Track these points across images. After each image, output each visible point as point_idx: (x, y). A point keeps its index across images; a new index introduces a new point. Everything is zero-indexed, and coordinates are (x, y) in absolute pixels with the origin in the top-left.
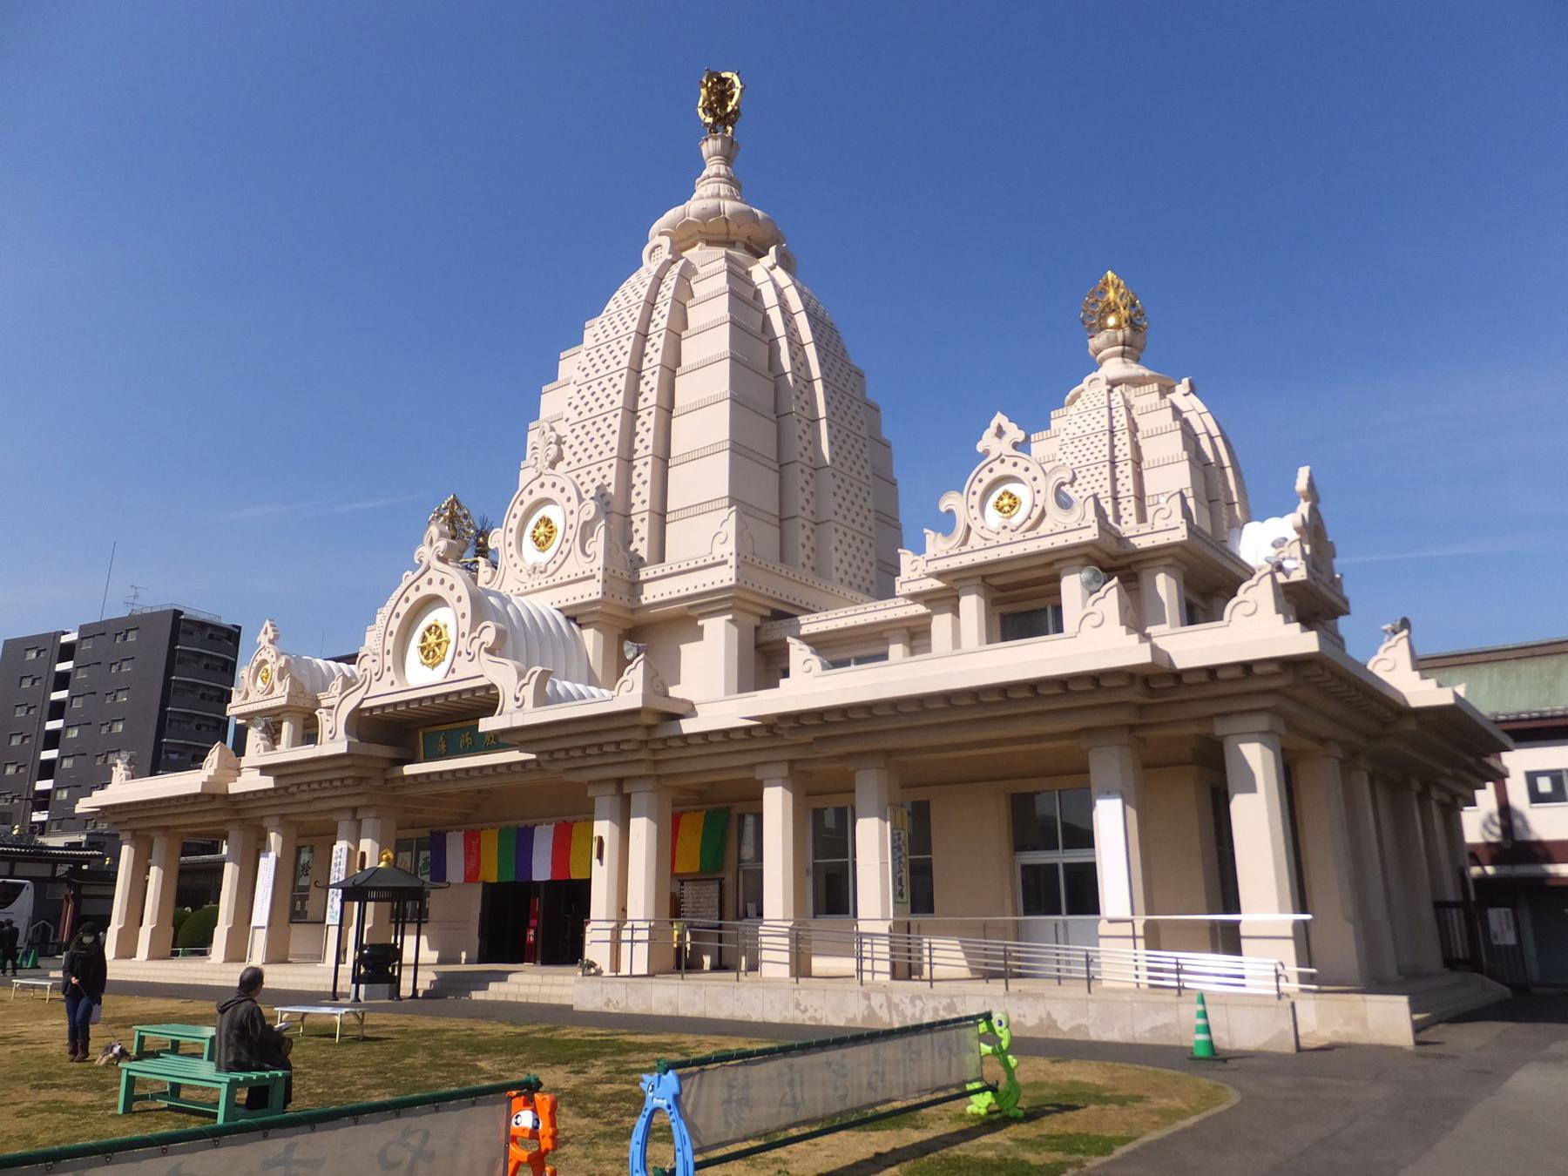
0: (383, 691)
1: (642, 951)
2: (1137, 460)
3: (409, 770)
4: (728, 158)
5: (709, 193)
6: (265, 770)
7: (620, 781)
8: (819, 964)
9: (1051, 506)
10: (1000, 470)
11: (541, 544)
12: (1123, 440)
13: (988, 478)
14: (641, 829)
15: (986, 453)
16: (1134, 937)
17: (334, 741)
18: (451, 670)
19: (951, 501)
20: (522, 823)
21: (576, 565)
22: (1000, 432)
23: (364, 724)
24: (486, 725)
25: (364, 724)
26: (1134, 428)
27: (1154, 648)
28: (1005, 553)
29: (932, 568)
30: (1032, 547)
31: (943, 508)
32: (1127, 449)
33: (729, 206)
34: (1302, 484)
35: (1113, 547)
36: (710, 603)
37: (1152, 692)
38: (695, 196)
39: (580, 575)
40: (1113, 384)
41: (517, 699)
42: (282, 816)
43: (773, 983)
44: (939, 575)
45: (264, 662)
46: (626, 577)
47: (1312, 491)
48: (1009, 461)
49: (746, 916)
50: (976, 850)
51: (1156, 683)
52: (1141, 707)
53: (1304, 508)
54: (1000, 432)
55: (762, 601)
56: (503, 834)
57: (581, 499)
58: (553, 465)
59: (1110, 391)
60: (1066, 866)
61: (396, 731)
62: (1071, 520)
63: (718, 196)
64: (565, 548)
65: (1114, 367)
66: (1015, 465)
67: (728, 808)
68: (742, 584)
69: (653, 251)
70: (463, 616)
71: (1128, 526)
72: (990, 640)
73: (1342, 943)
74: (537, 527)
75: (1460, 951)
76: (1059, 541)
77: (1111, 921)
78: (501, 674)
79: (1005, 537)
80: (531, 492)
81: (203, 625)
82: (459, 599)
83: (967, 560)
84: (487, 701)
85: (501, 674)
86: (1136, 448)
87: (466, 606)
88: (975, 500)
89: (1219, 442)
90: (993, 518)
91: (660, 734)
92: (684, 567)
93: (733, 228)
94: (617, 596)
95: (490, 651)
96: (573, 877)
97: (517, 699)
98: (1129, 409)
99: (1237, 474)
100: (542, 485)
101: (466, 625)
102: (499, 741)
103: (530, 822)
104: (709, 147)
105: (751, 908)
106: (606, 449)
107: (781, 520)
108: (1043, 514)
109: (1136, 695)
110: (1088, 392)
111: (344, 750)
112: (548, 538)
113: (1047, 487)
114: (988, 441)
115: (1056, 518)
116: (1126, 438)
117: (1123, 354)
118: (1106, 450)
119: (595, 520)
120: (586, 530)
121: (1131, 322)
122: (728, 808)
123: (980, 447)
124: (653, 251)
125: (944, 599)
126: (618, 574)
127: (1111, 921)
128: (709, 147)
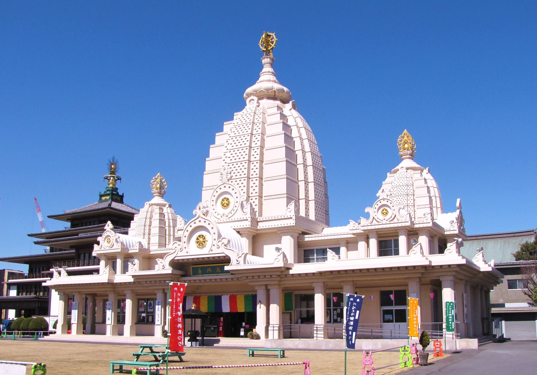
1: (276, 333)
4: (272, 65)
5: (267, 80)
6: (133, 276)
10: (383, 202)
13: (380, 204)
17: (163, 268)
21: (239, 215)
23: (177, 265)
24: (226, 268)
25: (177, 265)
28: (384, 226)
29: (363, 228)
30: (111, 251)
31: (366, 211)
33: (267, 80)
34: (458, 204)
40: (407, 169)
42: (132, 290)
44: (364, 230)
45: (108, 236)
47: (460, 207)
49: (297, 323)
51: (111, 285)
52: (423, 273)
53: (458, 211)
54: (108, 226)
56: (209, 298)
60: (395, 310)
61: (182, 267)
63: (270, 81)
64: (235, 209)
67: (292, 293)
69: (250, 101)
75: (486, 331)
79: (384, 222)
90: (380, 216)
91: (285, 273)
93: (277, 94)
96: (239, 311)
100: (225, 187)
103: (220, 294)
106: (243, 174)
109: (423, 271)
110: (400, 171)
111: (171, 272)
112: (228, 205)
122: (292, 293)
123: (377, 195)
124: (250, 101)
125: (366, 237)
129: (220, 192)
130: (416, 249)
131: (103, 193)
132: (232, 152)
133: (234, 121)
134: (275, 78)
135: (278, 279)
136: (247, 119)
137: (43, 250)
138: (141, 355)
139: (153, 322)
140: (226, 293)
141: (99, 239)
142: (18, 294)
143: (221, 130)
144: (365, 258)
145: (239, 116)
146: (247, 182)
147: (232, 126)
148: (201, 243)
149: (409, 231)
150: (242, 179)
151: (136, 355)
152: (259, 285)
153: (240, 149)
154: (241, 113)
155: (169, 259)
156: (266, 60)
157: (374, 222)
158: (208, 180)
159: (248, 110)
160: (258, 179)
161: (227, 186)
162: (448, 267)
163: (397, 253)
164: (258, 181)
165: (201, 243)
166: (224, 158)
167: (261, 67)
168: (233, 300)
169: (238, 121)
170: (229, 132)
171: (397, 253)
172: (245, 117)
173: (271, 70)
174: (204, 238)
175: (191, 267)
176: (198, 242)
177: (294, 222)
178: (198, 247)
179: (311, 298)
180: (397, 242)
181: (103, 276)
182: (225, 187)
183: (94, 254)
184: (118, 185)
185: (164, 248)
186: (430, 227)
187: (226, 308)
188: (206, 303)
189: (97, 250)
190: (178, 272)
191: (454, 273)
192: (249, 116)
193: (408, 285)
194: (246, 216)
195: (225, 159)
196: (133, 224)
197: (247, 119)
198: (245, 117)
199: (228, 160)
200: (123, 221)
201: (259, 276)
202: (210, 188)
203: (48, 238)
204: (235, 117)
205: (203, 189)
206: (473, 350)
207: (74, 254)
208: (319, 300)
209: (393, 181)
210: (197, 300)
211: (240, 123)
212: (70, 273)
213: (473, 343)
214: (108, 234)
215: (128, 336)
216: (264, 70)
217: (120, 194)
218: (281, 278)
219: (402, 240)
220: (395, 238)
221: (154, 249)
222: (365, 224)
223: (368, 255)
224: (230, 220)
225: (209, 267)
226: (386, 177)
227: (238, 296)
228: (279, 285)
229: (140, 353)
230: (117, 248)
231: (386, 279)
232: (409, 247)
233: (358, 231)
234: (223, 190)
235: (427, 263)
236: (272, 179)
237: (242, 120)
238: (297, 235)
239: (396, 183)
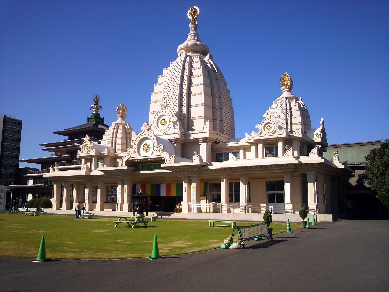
0: (135, 157)
3: (142, 172)
4: (195, 28)
5: (190, 40)
6: (102, 171)
8: (105, 210)
9: (278, 129)
10: (268, 121)
11: (164, 124)
13: (265, 122)
14: (194, 185)
15: (265, 118)
16: (291, 206)
17: (122, 166)
18: (152, 153)
19: (258, 126)
21: (172, 130)
22: (87, 138)
23: (129, 163)
24: (162, 165)
25: (129, 163)
28: (268, 137)
29: (254, 139)
30: (274, 137)
31: (256, 128)
34: (321, 122)
35: (288, 137)
36: (203, 140)
37: (296, 167)
38: (188, 39)
39: (172, 133)
40: (286, 98)
41: (170, 161)
43: (225, 214)
44: (255, 140)
45: (87, 144)
46: (183, 133)
47: (323, 124)
48: (269, 120)
50: (261, 190)
53: (322, 126)
54: (87, 138)
55: (212, 139)
57: (173, 116)
58: (165, 107)
59: (286, 100)
61: (135, 165)
64: (170, 126)
65: (286, 94)
66: (271, 120)
68: (210, 137)
69: (181, 54)
70: (155, 143)
73: (323, 206)
74: (162, 120)
76: (279, 136)
77: (287, 204)
78: (166, 155)
80: (160, 113)
81: (12, 120)
82: (153, 139)
83: (261, 138)
84: (163, 161)
85: (166, 155)
87: (155, 140)
88: (263, 126)
91: (201, 169)
92: (199, 132)
94: (182, 137)
95: (162, 150)
97: (170, 161)
98: (290, 104)
100: (163, 112)
101: (156, 144)
102: (164, 168)
103: (159, 183)
104: (191, 26)
106: (175, 103)
107: (213, 120)
108: (276, 131)
114: (265, 115)
115: (279, 132)
119: (177, 121)
120: (175, 123)
123: (264, 116)
124: (181, 54)
126: (182, 133)
127: (287, 204)
128: (191, 26)
129: (159, 115)
130: (290, 151)
131: (90, 117)
132: (168, 88)
133: (170, 68)
135: (197, 173)
136: (178, 66)
137: (49, 155)
138: (119, 222)
139: (96, 202)
141: (81, 147)
142: (34, 183)
143: (162, 74)
144: (253, 159)
145: (173, 64)
146: (165, 111)
147: (168, 70)
149: (286, 141)
150: (175, 107)
151: (116, 222)
153: (171, 87)
154: (175, 62)
155: (125, 159)
158: (154, 107)
159: (180, 60)
160: (285, 116)
162: (311, 165)
163: (277, 155)
164: (285, 117)
166: (163, 92)
167: (190, 31)
168: (168, 187)
169: (173, 67)
170: (167, 75)
171: (277, 155)
172: (177, 65)
177: (209, 135)
178: (147, 152)
179: (219, 186)
180: (277, 148)
184: (100, 112)
185: (125, 153)
186: (300, 138)
187: (163, 193)
188: (150, 188)
189: (79, 154)
190: (132, 168)
191: (315, 169)
192: (180, 64)
194: (177, 131)
195: (164, 93)
196: (104, 137)
197: (178, 66)
198: (177, 65)
199: (165, 94)
200: (97, 134)
201: (184, 171)
202: (153, 112)
203: (50, 147)
204: (171, 65)
205: (150, 113)
206: (328, 223)
207: (69, 157)
208: (223, 186)
209: (277, 107)
210: (143, 187)
211: (174, 69)
213: (329, 218)
214: (87, 143)
215: (97, 211)
216: (191, 32)
217: (102, 118)
218: (199, 172)
220: (276, 145)
221: (119, 154)
222: (255, 136)
223: (257, 156)
224: (166, 134)
227: (171, 185)
228: (198, 177)
229: (118, 221)
230: (93, 153)
231: (256, 174)
232: (285, 151)
233: (251, 141)
234: (162, 114)
236: (196, 106)
237: (175, 67)
238: (211, 144)
239: (278, 108)
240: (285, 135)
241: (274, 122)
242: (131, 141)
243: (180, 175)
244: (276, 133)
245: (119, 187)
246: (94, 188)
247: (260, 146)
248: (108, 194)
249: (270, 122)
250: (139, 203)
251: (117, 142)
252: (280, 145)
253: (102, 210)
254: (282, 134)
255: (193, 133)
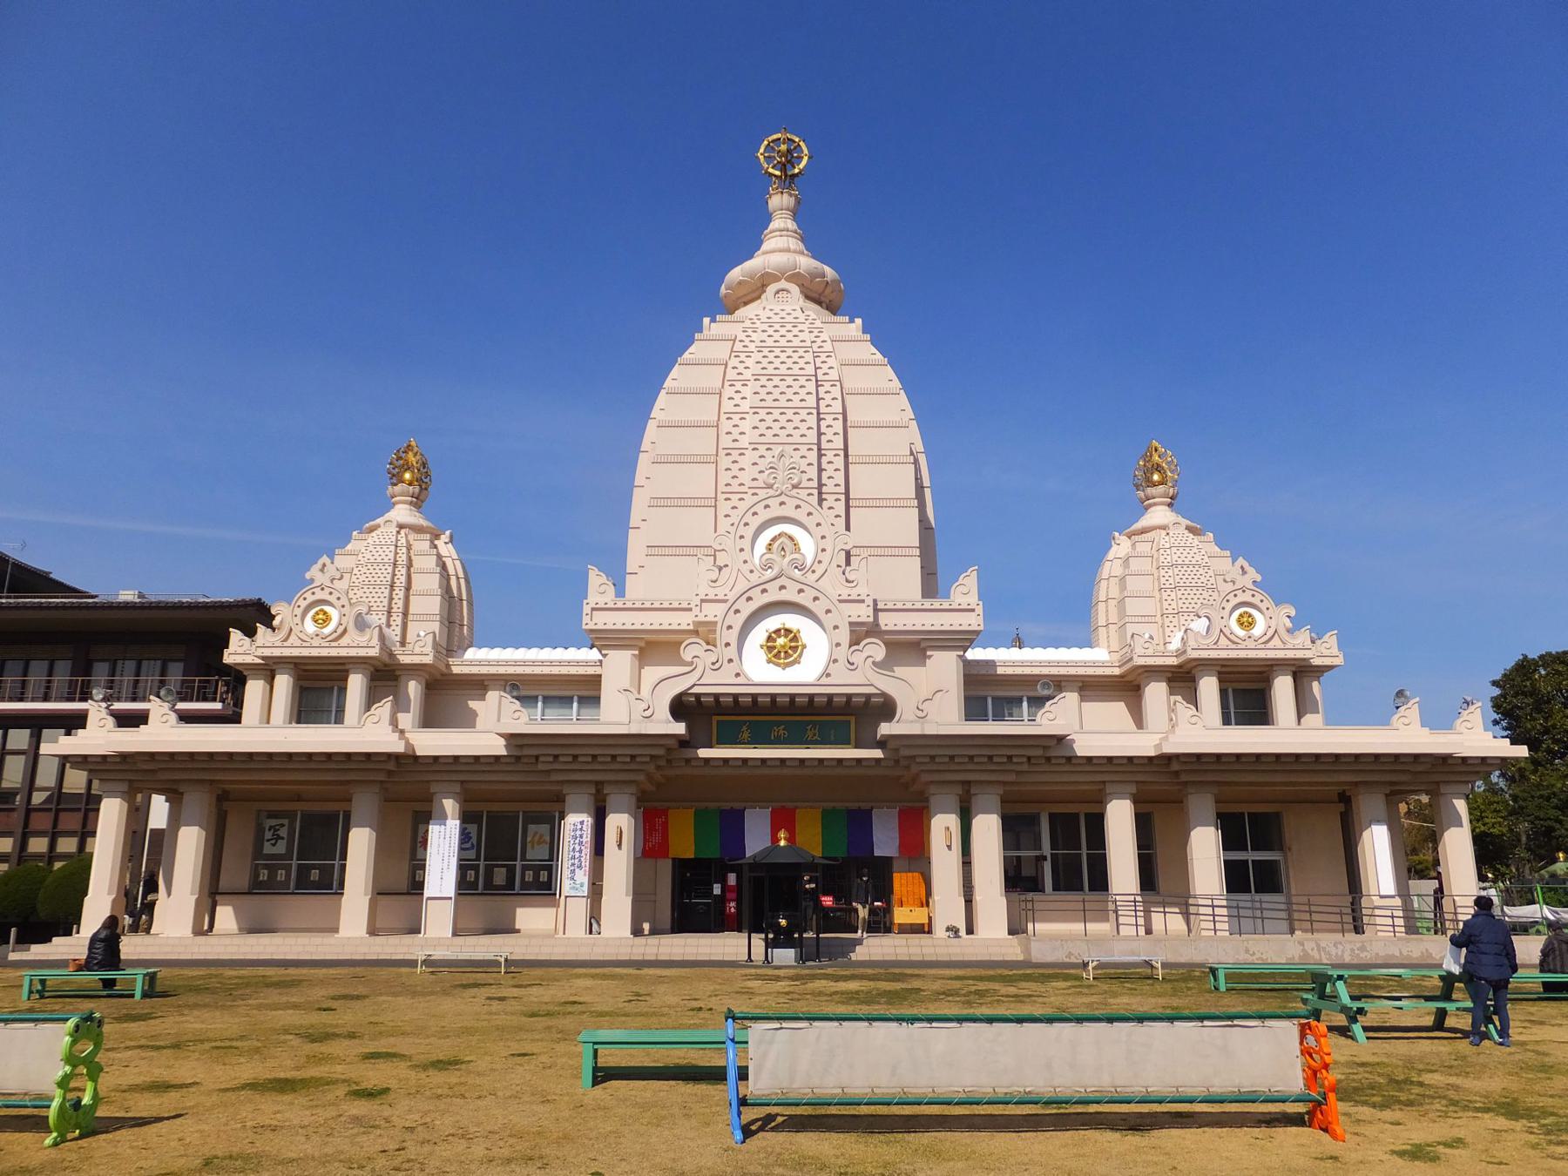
2: (408, 588)
3: (703, 753)
4: (796, 213)
5: (781, 247)
7: (599, 785)
9: (351, 627)
10: (320, 595)
12: (402, 572)
13: (311, 598)
15: (312, 581)
20: (727, 806)
24: (885, 729)
26: (410, 565)
27: (408, 743)
28: (315, 653)
29: (260, 652)
30: (334, 653)
32: (403, 579)
33: (781, 247)
35: (386, 659)
38: (765, 247)
40: (401, 527)
44: (263, 658)
51: (405, 762)
52: (390, 773)
62: (362, 639)
63: (788, 250)
65: (402, 512)
71: (397, 650)
72: (1226, 721)
76: (353, 653)
79: (1251, 644)
80: (798, 507)
83: (287, 652)
86: (410, 559)
88: (299, 612)
89: (462, 581)
90: (310, 627)
98: (409, 548)
99: (470, 604)
102: (881, 744)
103: (737, 806)
105: (327, 872)
108: (345, 631)
113: (351, 614)
114: (314, 572)
115: (353, 637)
116: (404, 571)
117: (411, 503)
118: (389, 578)
121: (420, 480)
123: (308, 576)
130: (384, 708)
134: (801, 246)
140: (759, 802)
148: (785, 649)
152: (617, 782)
156: (779, 201)
157: (1224, 642)
161: (792, 503)
163: (339, 719)
165: (785, 649)
167: (768, 218)
171: (339, 719)
173: (791, 225)
174: (795, 639)
175: (715, 718)
176: (770, 649)
177: (981, 620)
181: (266, 727)
182: (782, 503)
183: (229, 658)
193: (350, 800)
194: (717, 591)
212: (187, 718)
216: (773, 226)
219: (1283, 688)
220: (341, 684)
225: (779, 724)
226: (348, 540)
227: (799, 814)
235: (399, 748)
236: (893, 503)
240: (374, 652)
241: (344, 601)
242: (586, 609)
243: (924, 777)
244: (344, 641)
245: (577, 824)
246: (286, 822)
247: (283, 682)
248: (268, 849)
249: (328, 597)
250: (690, 893)
251: (412, 610)
252: (356, 684)
253: (204, 925)
254: (364, 645)
255: (937, 606)
